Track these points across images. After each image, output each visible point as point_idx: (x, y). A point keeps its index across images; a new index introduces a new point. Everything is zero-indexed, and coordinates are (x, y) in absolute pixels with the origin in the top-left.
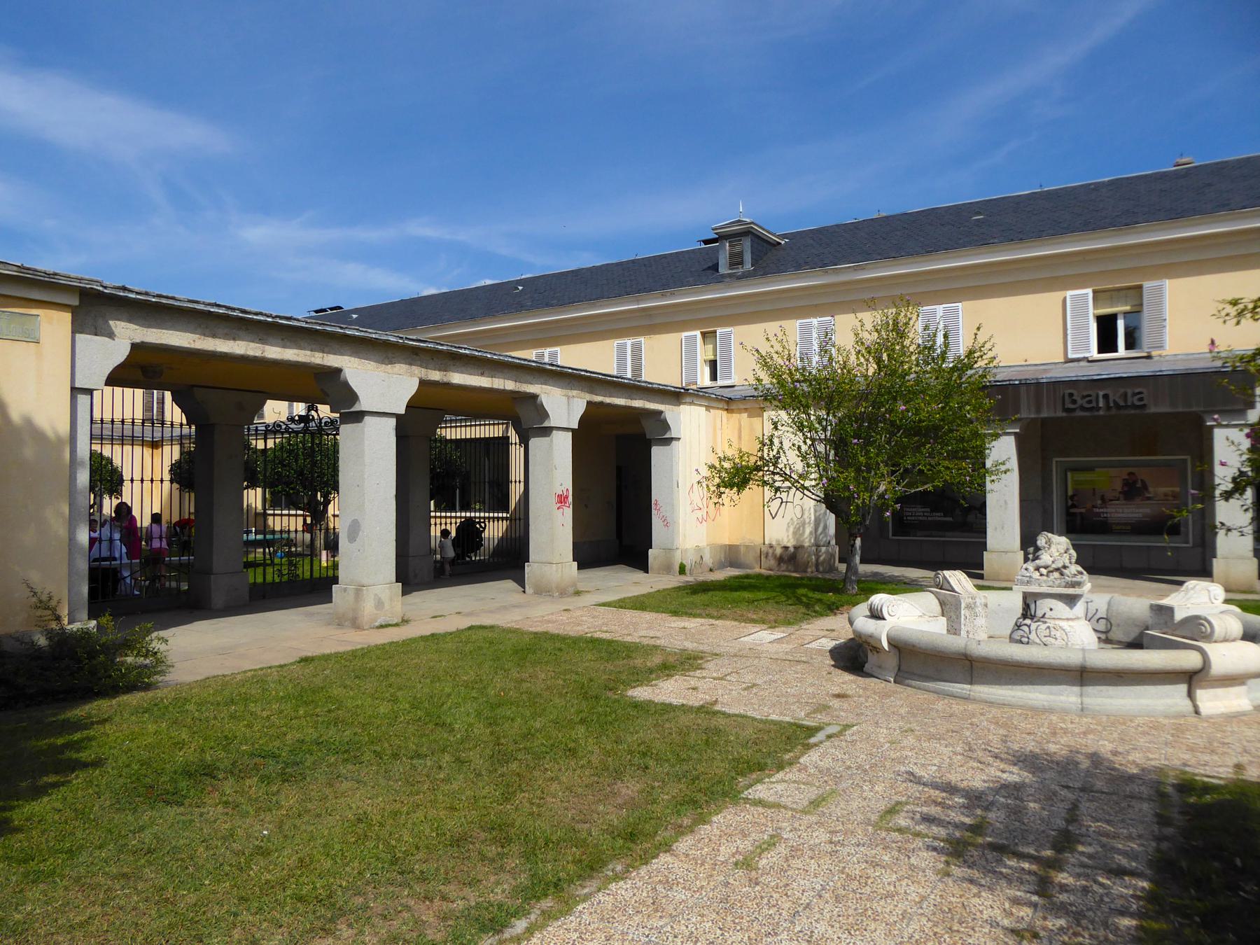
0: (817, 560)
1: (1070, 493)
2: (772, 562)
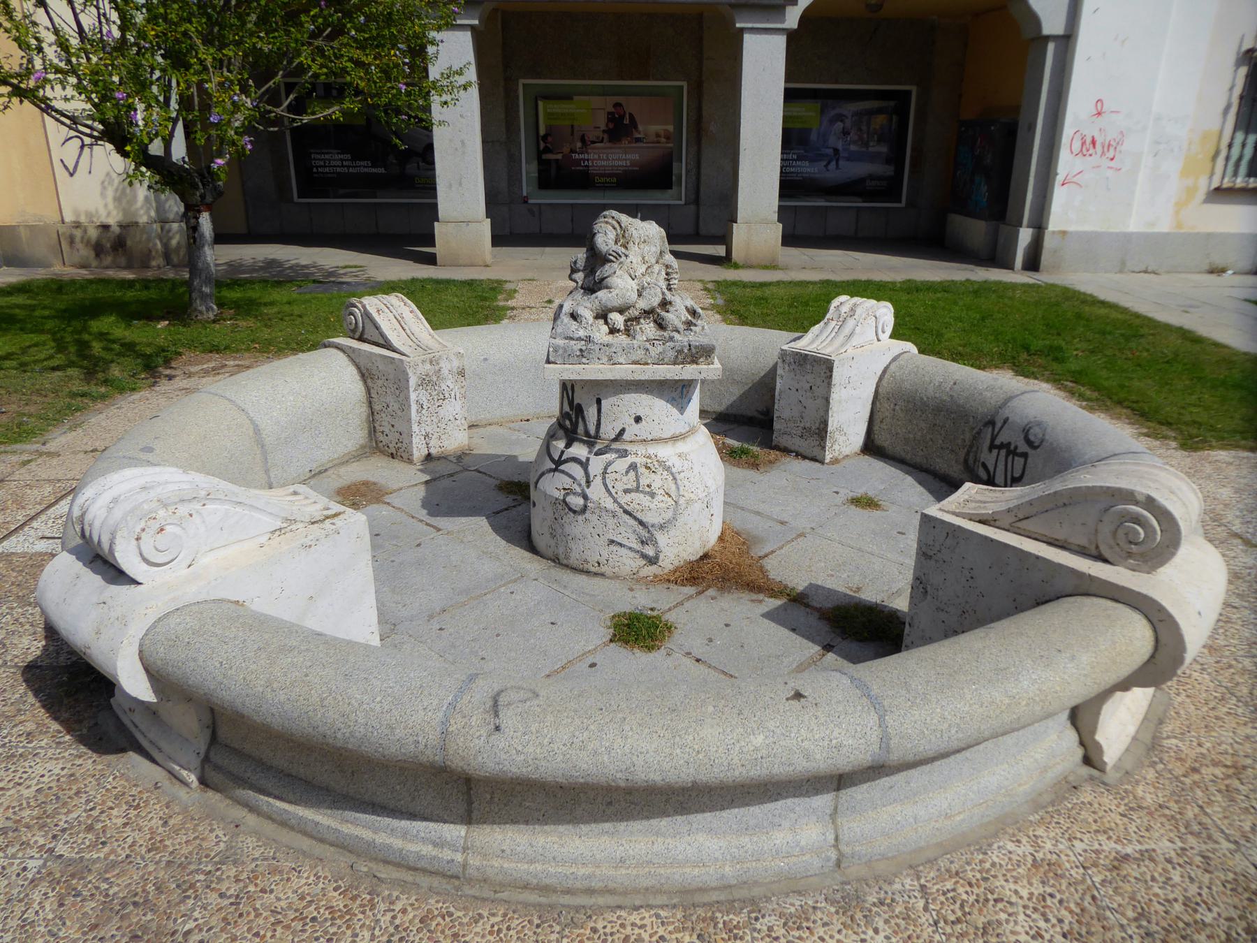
0: (166, 245)
1: (542, 132)
2: (85, 253)
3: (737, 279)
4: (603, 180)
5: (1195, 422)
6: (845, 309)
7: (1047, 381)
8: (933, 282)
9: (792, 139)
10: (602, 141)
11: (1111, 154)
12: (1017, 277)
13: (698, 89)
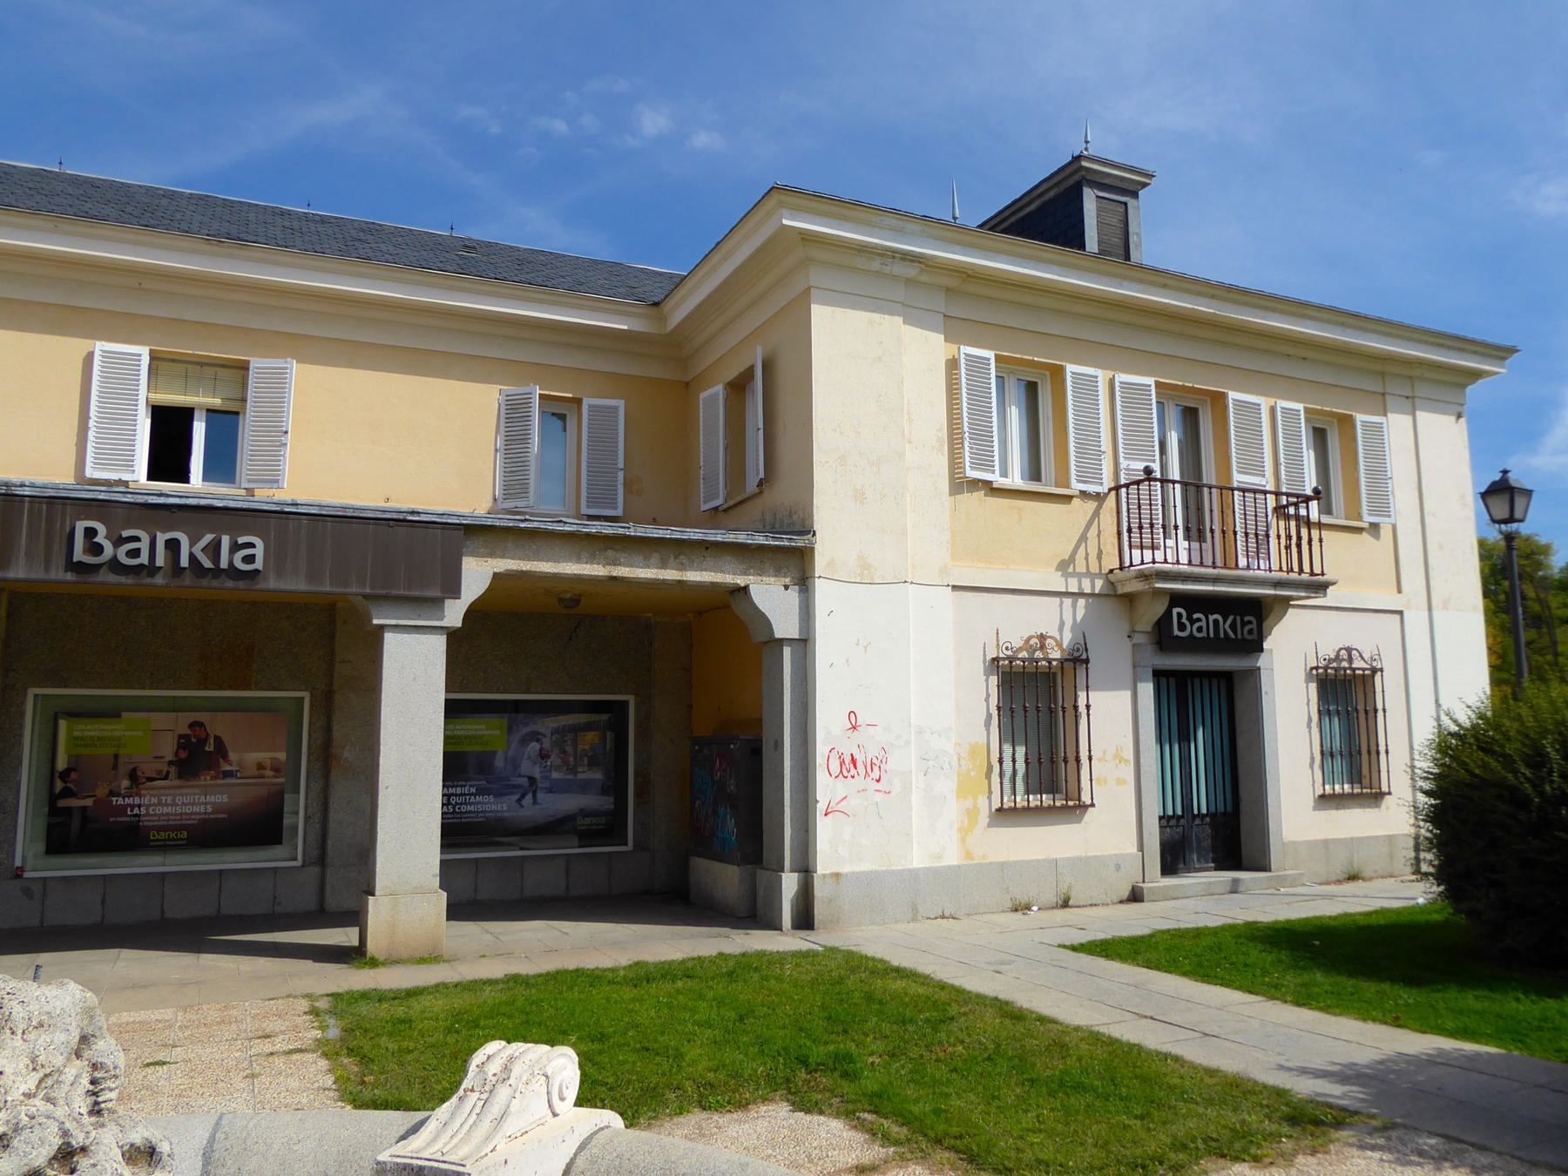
1: (61, 764)
3: (372, 985)
4: (163, 835)
5: (1039, 1161)
6: (494, 1068)
7: (837, 1115)
8: (671, 963)
9: (456, 766)
10: (166, 778)
11: (876, 775)
12: (785, 941)
13: (326, 704)
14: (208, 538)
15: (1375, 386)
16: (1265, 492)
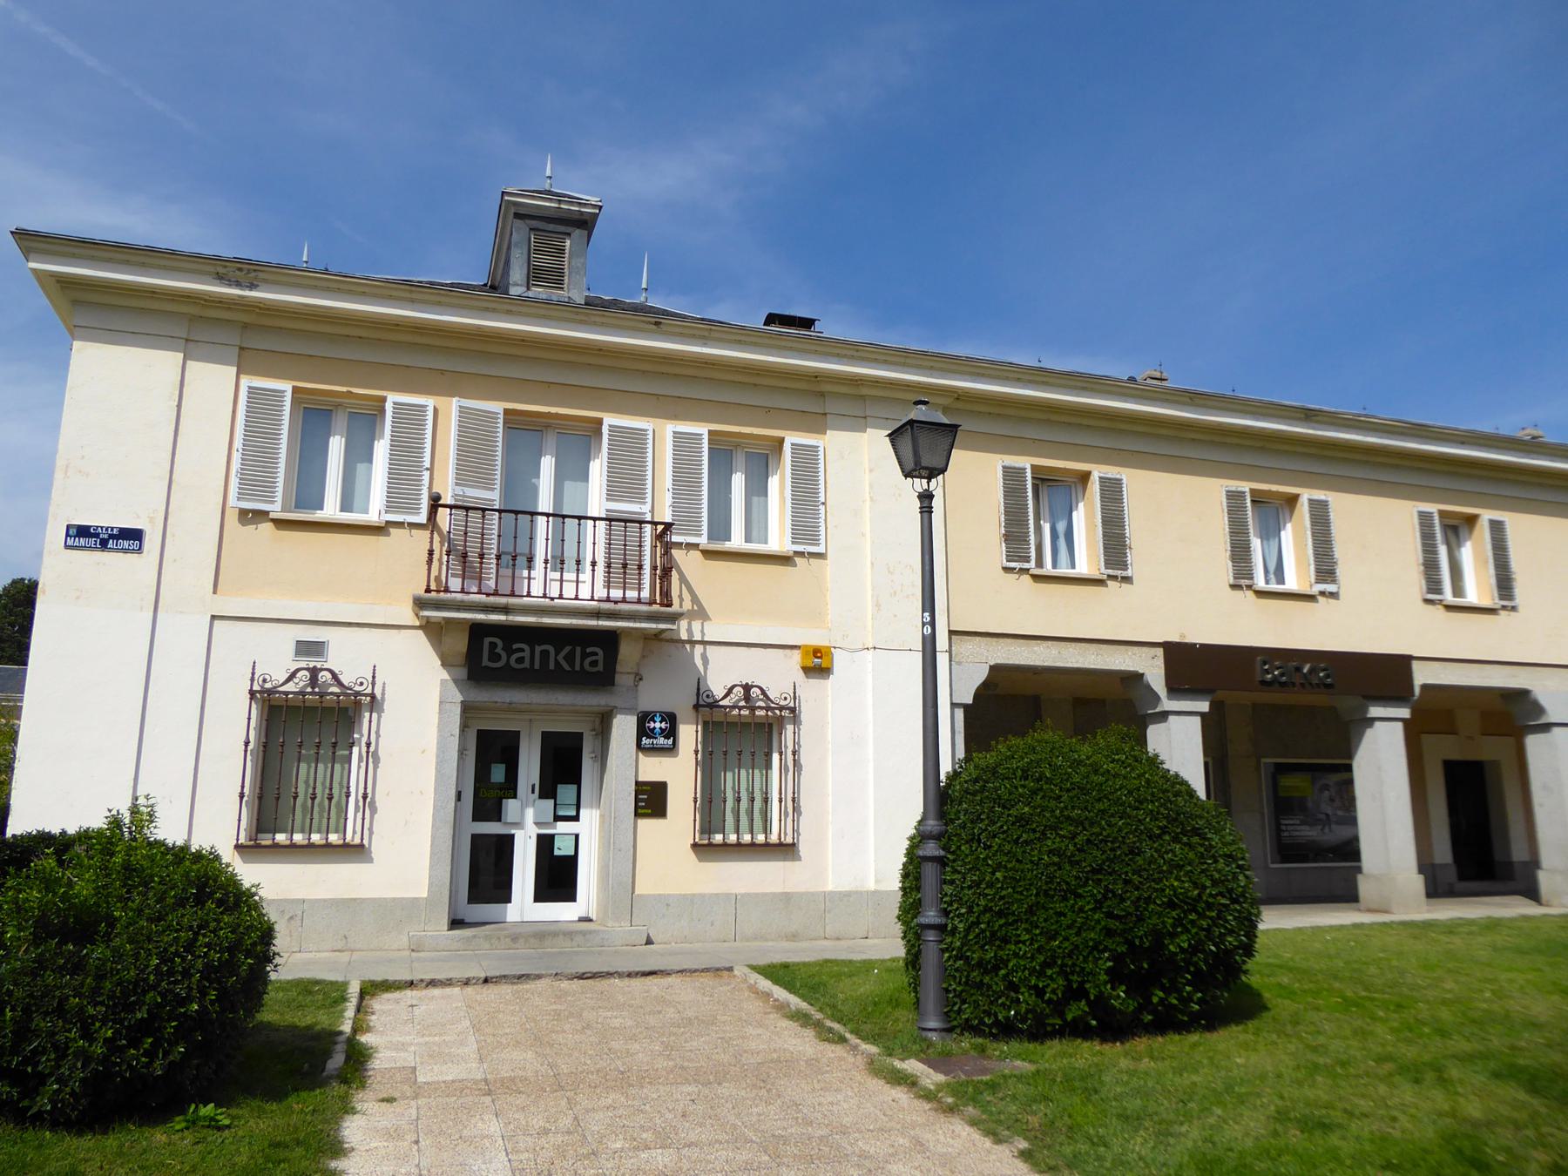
14: (568, 649)
15: (812, 406)
16: (641, 522)
